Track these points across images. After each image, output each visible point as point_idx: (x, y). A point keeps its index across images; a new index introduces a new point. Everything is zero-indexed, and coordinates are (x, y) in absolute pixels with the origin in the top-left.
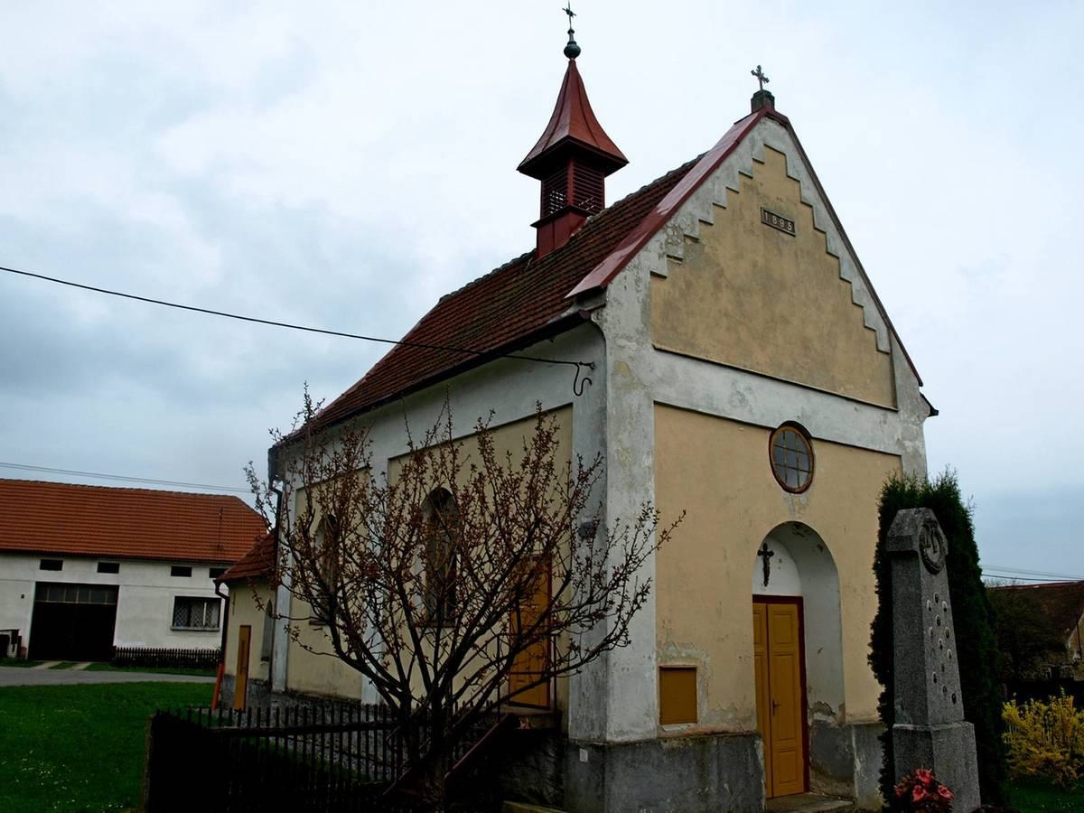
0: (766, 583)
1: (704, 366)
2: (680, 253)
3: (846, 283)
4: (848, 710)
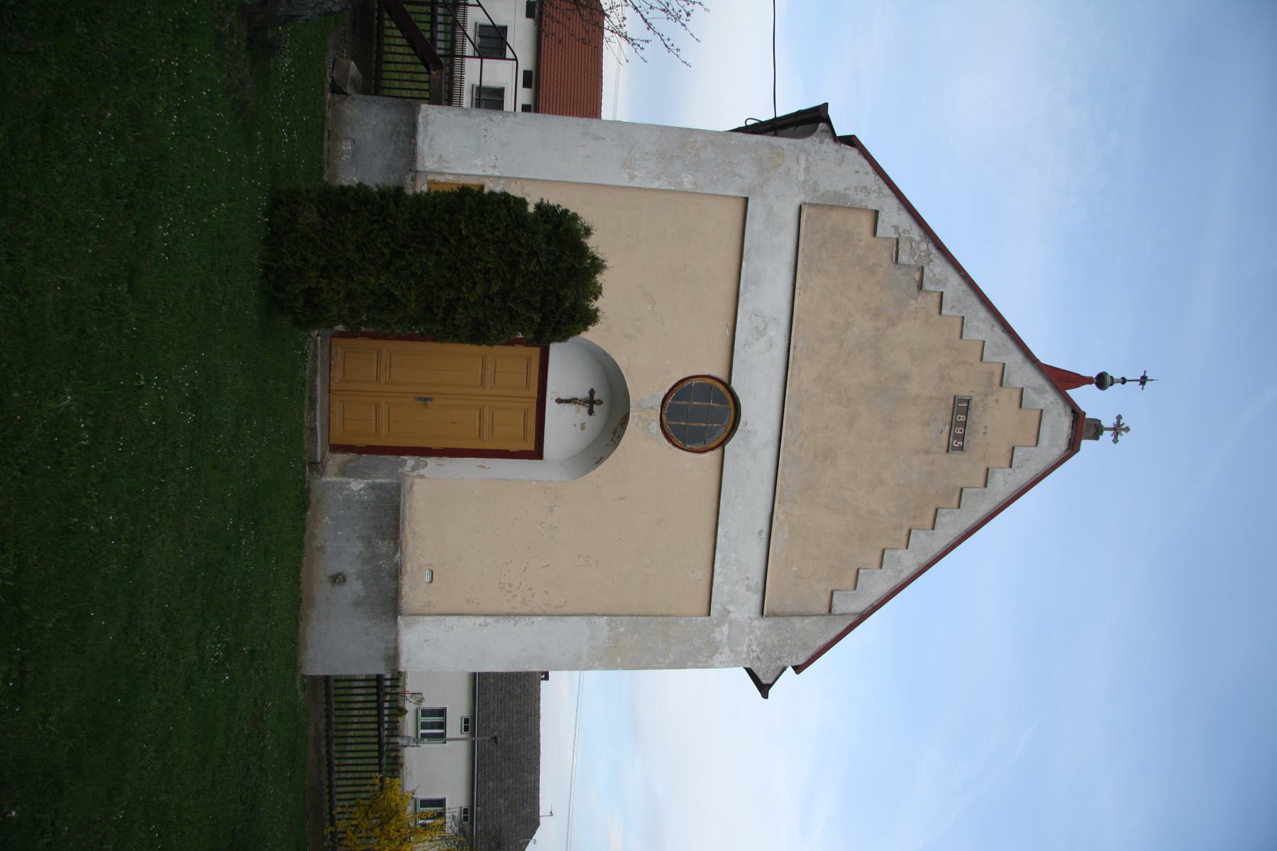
0: (559, 401)
1: (790, 275)
2: (903, 258)
3: (905, 539)
4: (417, 480)
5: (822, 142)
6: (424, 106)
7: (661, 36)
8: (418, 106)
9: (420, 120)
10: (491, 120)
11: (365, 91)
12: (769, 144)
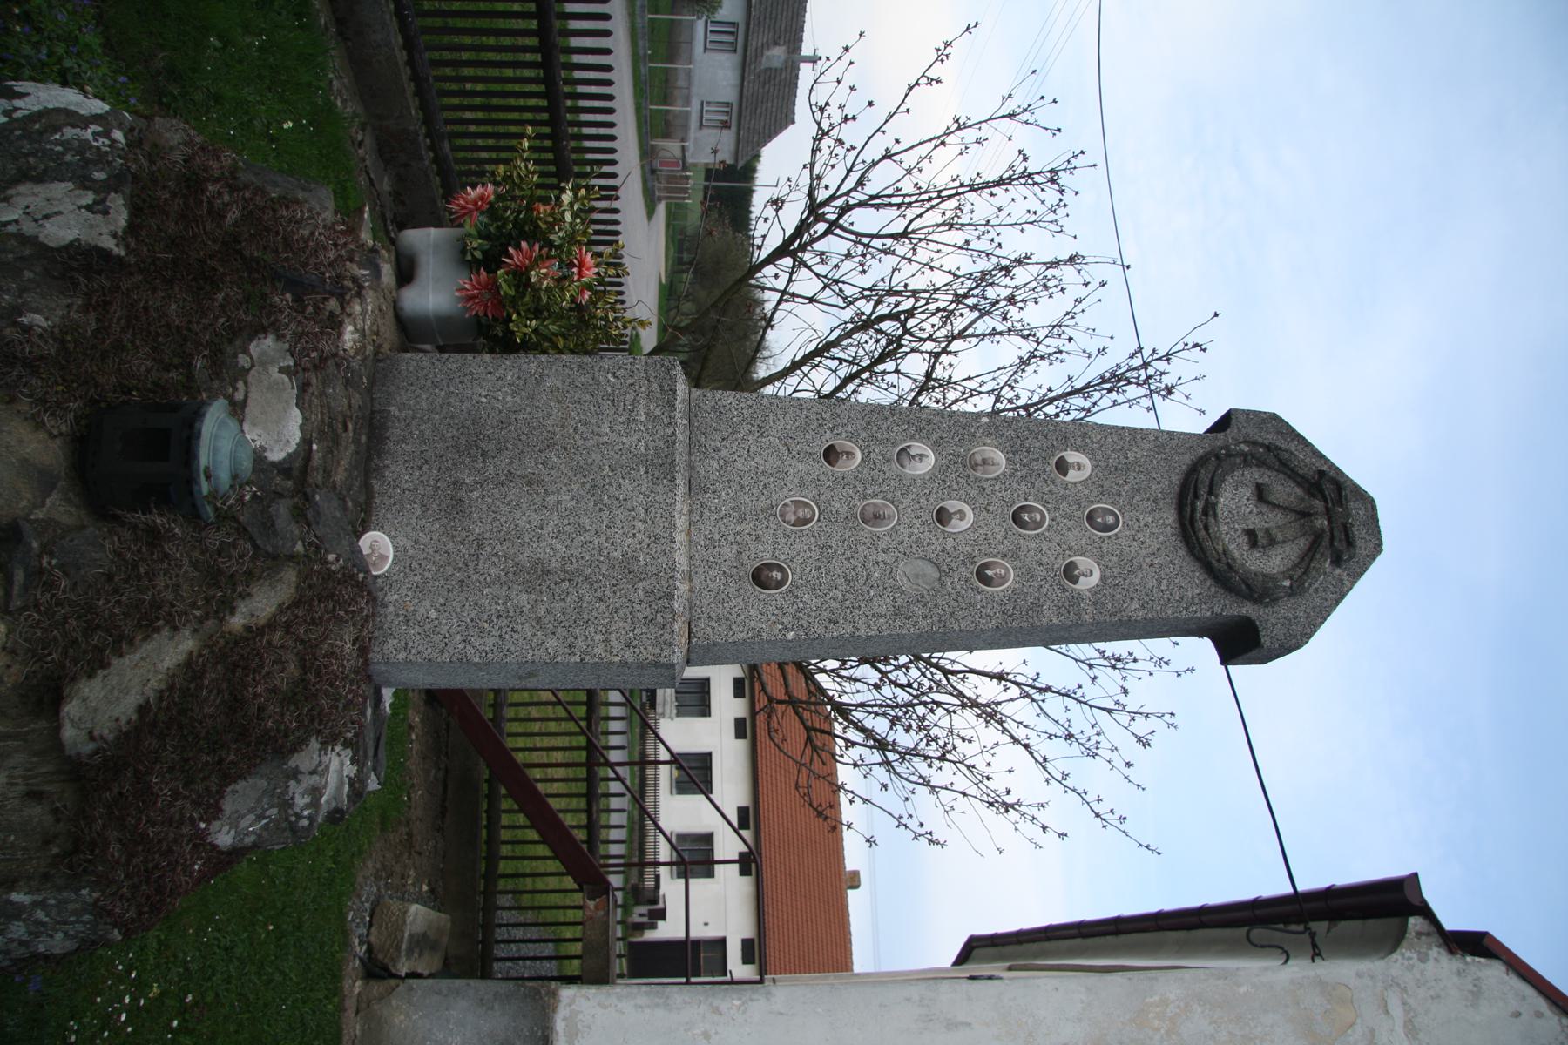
5: (1423, 959)
6: (567, 993)
7: (1082, 795)
8: (554, 994)
9: (560, 1025)
10: (717, 1011)
11: (452, 968)
12: (1320, 983)
